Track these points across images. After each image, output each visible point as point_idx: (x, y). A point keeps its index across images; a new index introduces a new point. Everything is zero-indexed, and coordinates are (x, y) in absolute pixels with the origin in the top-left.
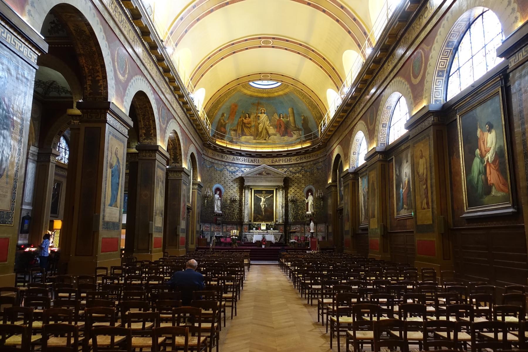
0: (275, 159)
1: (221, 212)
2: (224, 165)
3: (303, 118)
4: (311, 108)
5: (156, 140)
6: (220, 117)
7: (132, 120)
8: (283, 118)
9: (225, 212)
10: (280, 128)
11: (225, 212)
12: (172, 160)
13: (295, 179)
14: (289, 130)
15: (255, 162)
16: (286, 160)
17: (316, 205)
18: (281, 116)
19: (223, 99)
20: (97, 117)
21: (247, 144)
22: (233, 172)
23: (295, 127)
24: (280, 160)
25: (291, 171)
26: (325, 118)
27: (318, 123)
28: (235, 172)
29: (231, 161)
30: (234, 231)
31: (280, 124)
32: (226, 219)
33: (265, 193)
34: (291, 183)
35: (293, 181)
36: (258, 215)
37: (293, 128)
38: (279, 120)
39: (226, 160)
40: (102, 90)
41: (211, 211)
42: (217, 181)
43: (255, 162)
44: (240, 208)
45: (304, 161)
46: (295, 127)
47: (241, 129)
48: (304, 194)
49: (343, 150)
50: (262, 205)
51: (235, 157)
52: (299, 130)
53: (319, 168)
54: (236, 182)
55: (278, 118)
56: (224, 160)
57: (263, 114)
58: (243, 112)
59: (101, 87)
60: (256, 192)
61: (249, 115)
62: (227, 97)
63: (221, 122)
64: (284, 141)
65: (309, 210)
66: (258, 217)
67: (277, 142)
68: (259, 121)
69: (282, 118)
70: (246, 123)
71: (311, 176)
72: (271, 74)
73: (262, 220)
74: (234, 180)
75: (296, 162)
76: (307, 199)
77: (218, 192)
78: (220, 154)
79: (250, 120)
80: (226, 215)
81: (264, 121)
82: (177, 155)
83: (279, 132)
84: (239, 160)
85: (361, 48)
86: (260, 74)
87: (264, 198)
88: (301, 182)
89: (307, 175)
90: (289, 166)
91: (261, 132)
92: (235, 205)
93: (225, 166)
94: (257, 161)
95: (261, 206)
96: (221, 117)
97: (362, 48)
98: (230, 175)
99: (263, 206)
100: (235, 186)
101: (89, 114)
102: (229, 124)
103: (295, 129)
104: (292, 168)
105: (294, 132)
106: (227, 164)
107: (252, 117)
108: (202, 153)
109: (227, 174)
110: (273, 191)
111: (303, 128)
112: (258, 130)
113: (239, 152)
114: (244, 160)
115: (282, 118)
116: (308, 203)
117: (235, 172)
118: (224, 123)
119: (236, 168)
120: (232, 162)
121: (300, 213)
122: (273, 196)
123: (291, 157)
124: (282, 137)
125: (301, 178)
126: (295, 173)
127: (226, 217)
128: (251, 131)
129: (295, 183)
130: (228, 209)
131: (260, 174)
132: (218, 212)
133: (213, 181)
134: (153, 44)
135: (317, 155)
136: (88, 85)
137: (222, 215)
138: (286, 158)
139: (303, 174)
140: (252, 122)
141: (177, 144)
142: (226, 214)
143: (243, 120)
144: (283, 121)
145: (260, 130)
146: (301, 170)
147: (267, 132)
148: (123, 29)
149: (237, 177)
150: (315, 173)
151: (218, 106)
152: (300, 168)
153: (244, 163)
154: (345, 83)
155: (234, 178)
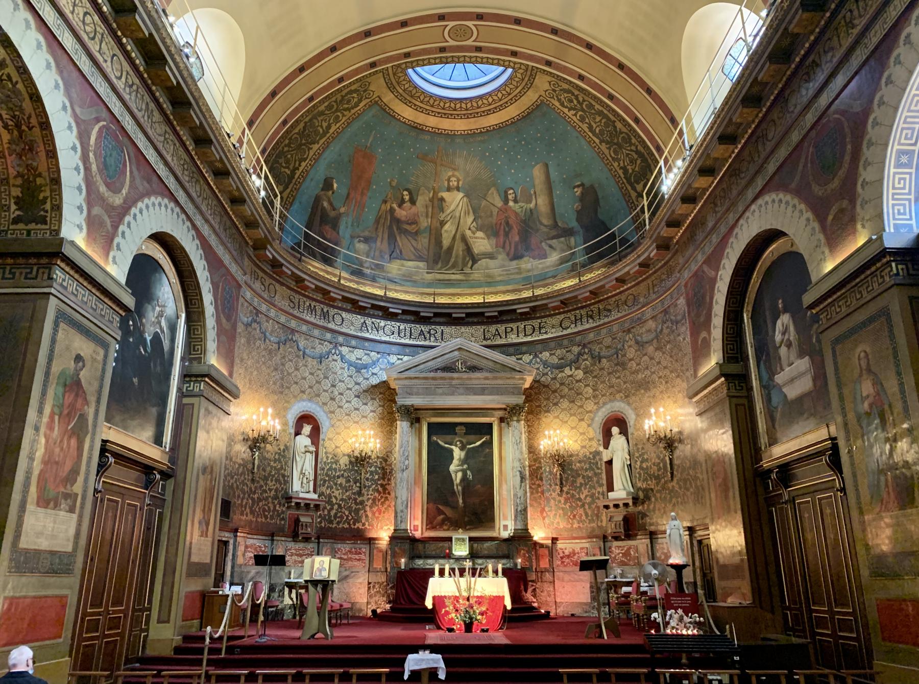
0: (492, 329)
1: (315, 496)
2: (331, 343)
3: (578, 191)
4: (606, 152)
5: (60, 222)
6: (317, 191)
7: (132, 294)
8: (516, 201)
9: (330, 496)
10: (507, 234)
11: (330, 496)
12: (13, 207)
13: (562, 384)
14: (534, 240)
15: (433, 339)
16: (529, 328)
17: (641, 468)
18: (510, 197)
19: (325, 125)
20: (29, 276)
21: (408, 286)
22: (359, 368)
23: (555, 225)
24: (509, 330)
25: (545, 364)
26: (681, 130)
27: (634, 194)
28: (366, 367)
29: (355, 330)
30: (318, 559)
31: (507, 223)
32: (331, 522)
33: (465, 434)
34: (548, 399)
35: (555, 391)
36: (441, 507)
37: (545, 230)
38: (505, 209)
39: (337, 328)
40: (47, 212)
41: (276, 490)
42: (303, 392)
43: (433, 339)
44: (382, 485)
45: (587, 326)
46: (555, 225)
47: (386, 236)
48: (595, 432)
49: (866, 112)
50: (456, 472)
51: (369, 321)
52: (568, 232)
53: (645, 338)
54: (372, 399)
55: (499, 203)
56: (331, 326)
57: (456, 192)
58: (394, 184)
59: (45, 203)
60: (434, 429)
61: (410, 193)
62: (337, 120)
63: (323, 208)
64: (519, 273)
65: (617, 484)
66: (440, 512)
67: (499, 279)
68: (442, 216)
69: (511, 204)
70: (403, 219)
71: (617, 371)
72: (480, 17)
73: (456, 525)
74: (364, 391)
75: (561, 334)
76: (606, 446)
77: (307, 429)
78: (319, 307)
79: (414, 210)
80: (332, 509)
81: (458, 215)
82: (39, 181)
83: (504, 247)
84: (381, 332)
85: (663, 152)
86: (442, 17)
87: (462, 449)
88: (581, 394)
89: (603, 369)
90: (539, 347)
91: (450, 248)
92: (366, 472)
93: (336, 345)
94: (438, 335)
95: (453, 476)
96: (322, 190)
97: (666, 153)
98: (351, 377)
99: (460, 475)
100: (368, 409)
101: (8, 268)
102: (350, 220)
103: (554, 233)
104: (547, 354)
105: (549, 242)
106: (341, 339)
107: (421, 200)
108: (242, 283)
109: (340, 372)
110: (490, 425)
111: (581, 227)
112: (439, 242)
113: (382, 304)
114: (396, 330)
115: (511, 204)
116: (610, 463)
117: (366, 367)
118: (332, 214)
119: (373, 354)
120: (359, 334)
121: (582, 497)
122: (489, 443)
123: (544, 320)
124: (514, 263)
125: (580, 381)
126: (560, 367)
127: (334, 511)
128: (420, 247)
129: (562, 397)
130: (341, 485)
131: (449, 368)
132: (302, 495)
133: (289, 388)
134: (237, 194)
135: (635, 299)
136: (14, 197)
137: (317, 507)
138: (526, 323)
139: (587, 367)
140: (422, 219)
141: (34, 121)
142: (332, 505)
143: (392, 210)
144: (516, 213)
145: (446, 242)
146: (580, 354)
147: (468, 249)
148: (164, 153)
149: (375, 381)
150: (631, 360)
151: (309, 149)
152: (576, 349)
153: (398, 341)
154: (683, 124)
155: (365, 385)
